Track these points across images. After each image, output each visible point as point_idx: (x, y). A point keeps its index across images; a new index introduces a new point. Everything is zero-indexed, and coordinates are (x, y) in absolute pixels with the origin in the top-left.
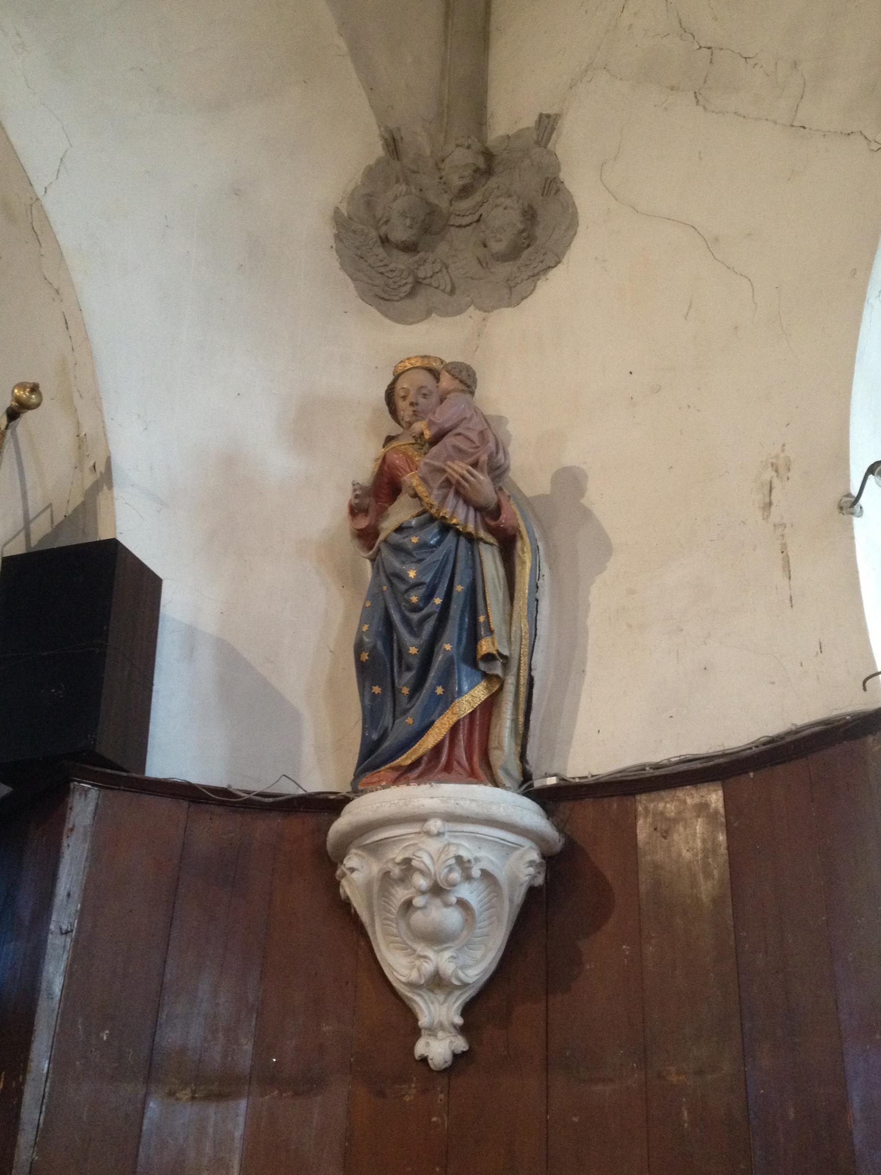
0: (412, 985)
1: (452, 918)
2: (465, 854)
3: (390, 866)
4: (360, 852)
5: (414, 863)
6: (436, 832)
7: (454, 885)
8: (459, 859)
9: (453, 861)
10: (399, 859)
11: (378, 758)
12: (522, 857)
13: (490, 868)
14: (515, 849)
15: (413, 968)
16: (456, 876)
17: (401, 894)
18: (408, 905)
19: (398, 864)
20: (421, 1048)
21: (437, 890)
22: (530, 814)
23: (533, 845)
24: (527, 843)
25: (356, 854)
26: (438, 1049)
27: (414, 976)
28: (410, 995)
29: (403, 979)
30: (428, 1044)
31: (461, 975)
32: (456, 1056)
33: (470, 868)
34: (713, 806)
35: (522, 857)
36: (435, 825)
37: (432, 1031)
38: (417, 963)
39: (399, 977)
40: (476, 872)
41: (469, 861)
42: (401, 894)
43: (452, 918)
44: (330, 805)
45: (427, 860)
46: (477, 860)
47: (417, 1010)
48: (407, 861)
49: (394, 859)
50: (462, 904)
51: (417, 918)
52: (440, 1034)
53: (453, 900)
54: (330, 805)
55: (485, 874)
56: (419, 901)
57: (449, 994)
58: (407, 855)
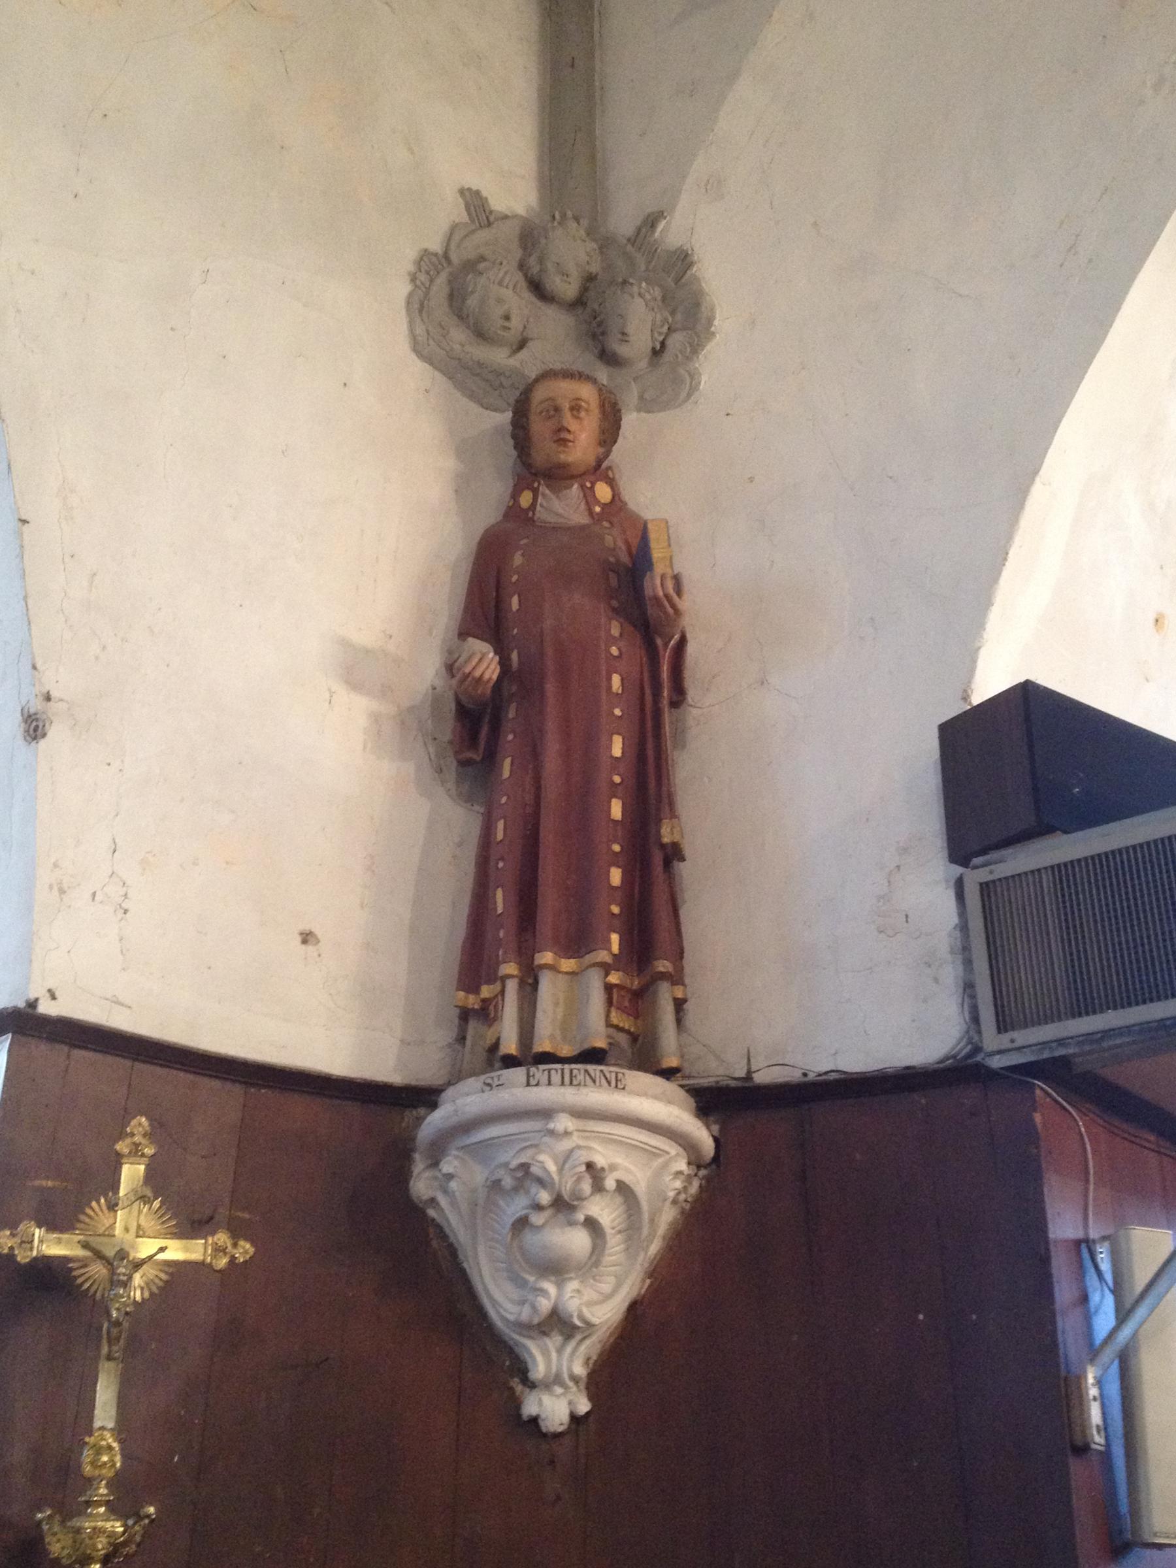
0: (527, 1328)
1: (577, 1241)
2: (600, 1161)
3: (501, 1173)
4: (460, 1154)
5: (535, 1170)
6: (672, 1062)
7: (581, 1199)
8: (590, 1166)
9: (583, 1168)
10: (514, 1163)
11: (479, 1039)
12: (665, 1165)
13: (627, 1179)
14: (659, 1156)
15: (522, 1303)
16: (586, 1186)
17: (516, 1207)
18: (522, 1223)
19: (513, 1170)
20: (531, 1406)
21: (563, 1205)
22: (676, 1112)
23: (680, 1150)
24: (673, 1149)
25: (457, 1157)
26: (555, 1407)
27: (525, 1314)
28: (517, 1337)
29: (511, 1318)
30: (540, 1402)
31: (585, 1311)
32: (574, 1418)
33: (603, 1179)
34: (84, 1536)
35: (665, 1165)
36: (563, 1122)
37: (547, 1385)
38: (530, 1297)
39: (504, 1313)
40: (610, 1183)
41: (603, 1169)
42: (516, 1207)
43: (577, 1241)
44: (423, 1097)
45: (552, 1167)
46: (613, 1167)
47: (529, 1360)
48: (525, 1167)
49: (506, 1165)
50: (591, 1224)
51: (530, 1239)
52: (559, 1390)
53: (581, 1217)
54: (423, 1097)
55: (622, 1188)
56: (537, 1219)
57: (568, 1337)
58: (523, 1159)
